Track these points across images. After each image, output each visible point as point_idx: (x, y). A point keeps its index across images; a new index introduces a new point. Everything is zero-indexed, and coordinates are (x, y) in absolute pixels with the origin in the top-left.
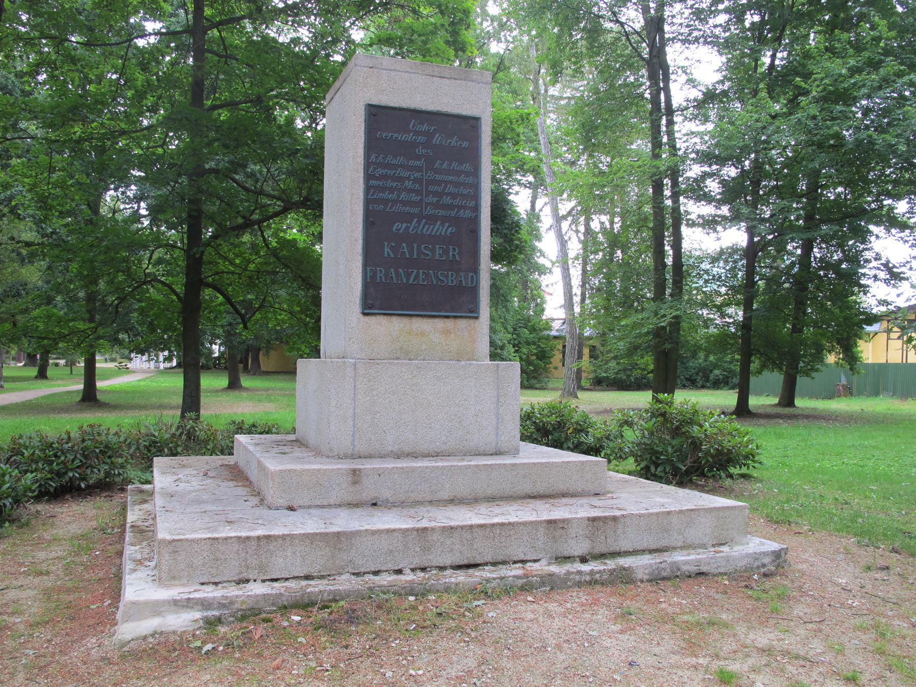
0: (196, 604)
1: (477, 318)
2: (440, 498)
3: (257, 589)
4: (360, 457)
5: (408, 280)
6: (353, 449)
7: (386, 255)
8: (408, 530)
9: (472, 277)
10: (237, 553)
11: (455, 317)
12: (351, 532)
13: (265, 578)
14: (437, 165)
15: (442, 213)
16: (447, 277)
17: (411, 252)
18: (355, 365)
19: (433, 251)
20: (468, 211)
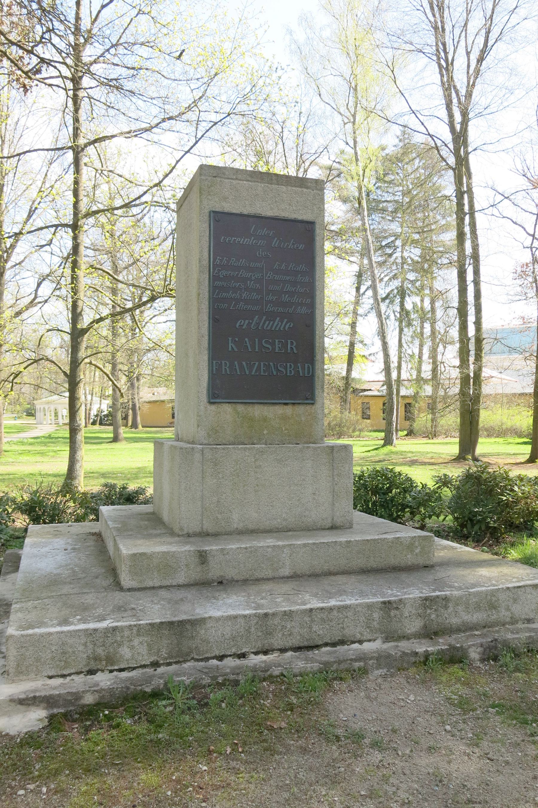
0: (41, 702)
1: (313, 404)
2: (282, 575)
3: (104, 680)
4: (208, 535)
5: (250, 372)
6: (202, 528)
7: (230, 349)
8: (250, 616)
9: (309, 367)
10: (85, 645)
11: (294, 404)
12: (196, 620)
13: (112, 668)
14: (276, 266)
15: (281, 310)
16: (286, 368)
17: (253, 347)
18: (202, 450)
19: (273, 344)
20: (304, 308)
